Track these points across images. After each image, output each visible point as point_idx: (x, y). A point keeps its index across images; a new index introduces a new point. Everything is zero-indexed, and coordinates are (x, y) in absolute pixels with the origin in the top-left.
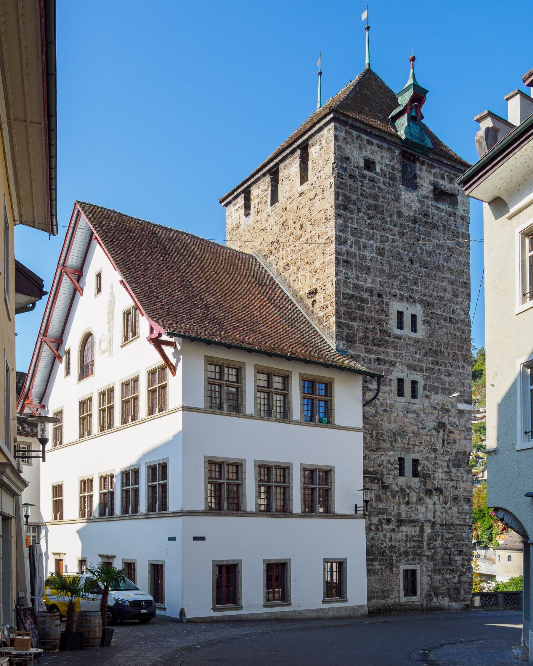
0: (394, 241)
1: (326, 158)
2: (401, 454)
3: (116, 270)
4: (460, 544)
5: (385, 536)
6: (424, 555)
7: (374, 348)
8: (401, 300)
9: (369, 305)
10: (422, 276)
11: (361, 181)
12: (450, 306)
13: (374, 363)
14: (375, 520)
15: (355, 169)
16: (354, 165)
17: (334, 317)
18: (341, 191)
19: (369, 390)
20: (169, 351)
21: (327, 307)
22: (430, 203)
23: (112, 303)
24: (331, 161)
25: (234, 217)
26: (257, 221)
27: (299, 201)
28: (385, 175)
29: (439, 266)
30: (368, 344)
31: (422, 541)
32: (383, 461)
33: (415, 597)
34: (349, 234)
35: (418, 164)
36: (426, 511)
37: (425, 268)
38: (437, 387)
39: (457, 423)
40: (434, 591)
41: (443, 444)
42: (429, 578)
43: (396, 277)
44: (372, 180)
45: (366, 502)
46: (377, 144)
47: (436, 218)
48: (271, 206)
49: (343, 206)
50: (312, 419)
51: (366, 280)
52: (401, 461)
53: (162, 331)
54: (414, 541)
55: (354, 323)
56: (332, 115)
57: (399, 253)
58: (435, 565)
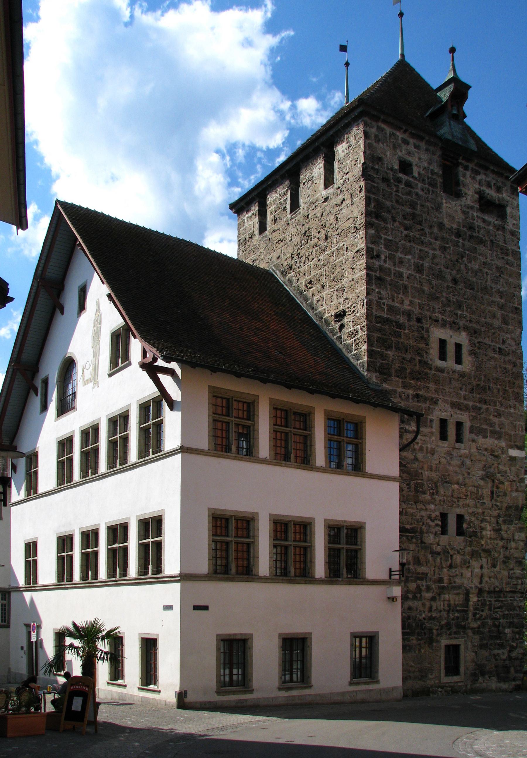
0: (434, 256)
1: (355, 157)
2: (443, 508)
3: (103, 283)
4: (511, 614)
5: (424, 605)
6: (469, 628)
7: (412, 382)
8: (444, 326)
9: (407, 331)
10: (467, 299)
11: (395, 186)
12: (499, 335)
13: (413, 399)
14: (412, 586)
15: (389, 171)
16: (387, 167)
17: (366, 344)
18: (372, 196)
19: (407, 431)
20: (166, 380)
21: (357, 332)
22: (475, 214)
23: (98, 322)
24: (360, 161)
25: (246, 225)
26: (274, 231)
27: (323, 207)
28: (424, 180)
29: (486, 288)
30: (406, 378)
31: (467, 611)
32: (422, 516)
33: (458, 677)
34: (382, 246)
35: (461, 169)
36: (471, 576)
37: (470, 289)
38: (486, 429)
39: (508, 471)
40: (480, 671)
41: (492, 497)
42: (473, 654)
43: (437, 298)
44: (408, 184)
45: (402, 565)
46: (414, 144)
47: (482, 231)
48: (291, 213)
49: (375, 214)
50: (339, 466)
51: (403, 301)
52: (444, 516)
53: (158, 354)
54: (458, 611)
55: (389, 352)
56: (361, 109)
57: (440, 271)
58: (481, 639)
